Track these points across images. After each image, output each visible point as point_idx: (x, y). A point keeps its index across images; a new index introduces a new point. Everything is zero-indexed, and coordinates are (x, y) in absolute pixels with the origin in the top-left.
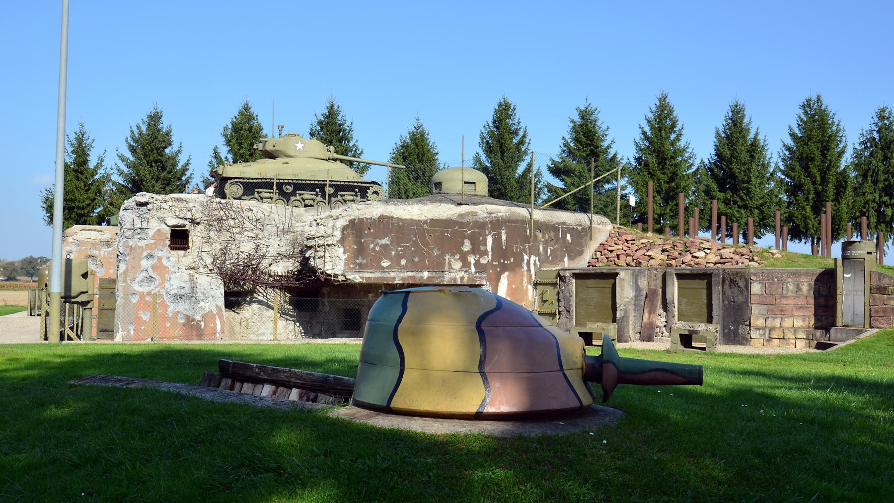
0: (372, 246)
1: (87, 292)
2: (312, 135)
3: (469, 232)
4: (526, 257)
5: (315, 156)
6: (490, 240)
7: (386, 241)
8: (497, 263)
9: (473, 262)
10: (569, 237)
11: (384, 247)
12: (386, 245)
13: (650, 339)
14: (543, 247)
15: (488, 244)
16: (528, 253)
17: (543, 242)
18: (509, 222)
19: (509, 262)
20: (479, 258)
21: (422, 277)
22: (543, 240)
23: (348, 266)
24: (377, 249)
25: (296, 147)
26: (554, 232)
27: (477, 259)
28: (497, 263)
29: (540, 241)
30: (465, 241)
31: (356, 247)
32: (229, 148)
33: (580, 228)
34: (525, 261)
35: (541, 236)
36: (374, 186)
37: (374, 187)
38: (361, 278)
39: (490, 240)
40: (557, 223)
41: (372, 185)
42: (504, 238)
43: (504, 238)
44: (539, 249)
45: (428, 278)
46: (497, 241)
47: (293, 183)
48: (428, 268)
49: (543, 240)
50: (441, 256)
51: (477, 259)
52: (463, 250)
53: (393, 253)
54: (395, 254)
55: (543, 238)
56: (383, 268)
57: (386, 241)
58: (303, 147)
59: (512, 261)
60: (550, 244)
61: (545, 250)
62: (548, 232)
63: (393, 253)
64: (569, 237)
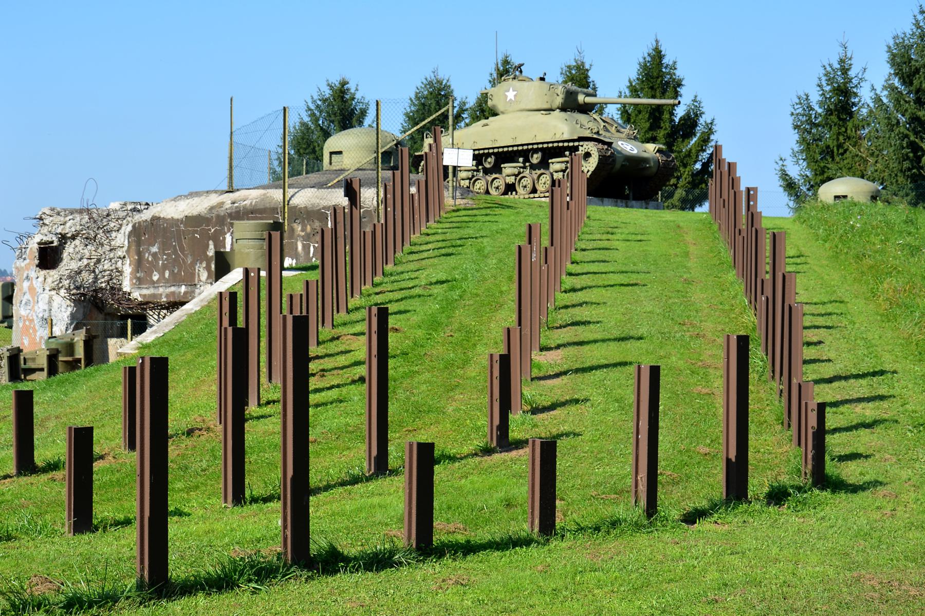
0: (147, 255)
1: (728, 336)
5: (535, 107)
11: (155, 255)
13: (365, 379)
14: (303, 244)
15: (226, 246)
17: (303, 237)
18: (252, 213)
21: (180, 293)
22: (303, 234)
26: (320, 221)
29: (299, 236)
35: (300, 229)
36: (585, 143)
37: (585, 146)
40: (324, 208)
41: (581, 143)
44: (297, 248)
45: (185, 293)
47: (493, 153)
48: (184, 281)
49: (303, 234)
50: (193, 264)
52: (208, 256)
53: (161, 262)
55: (302, 231)
58: (511, 99)
60: (313, 240)
61: (306, 248)
62: (311, 222)
63: (161, 262)
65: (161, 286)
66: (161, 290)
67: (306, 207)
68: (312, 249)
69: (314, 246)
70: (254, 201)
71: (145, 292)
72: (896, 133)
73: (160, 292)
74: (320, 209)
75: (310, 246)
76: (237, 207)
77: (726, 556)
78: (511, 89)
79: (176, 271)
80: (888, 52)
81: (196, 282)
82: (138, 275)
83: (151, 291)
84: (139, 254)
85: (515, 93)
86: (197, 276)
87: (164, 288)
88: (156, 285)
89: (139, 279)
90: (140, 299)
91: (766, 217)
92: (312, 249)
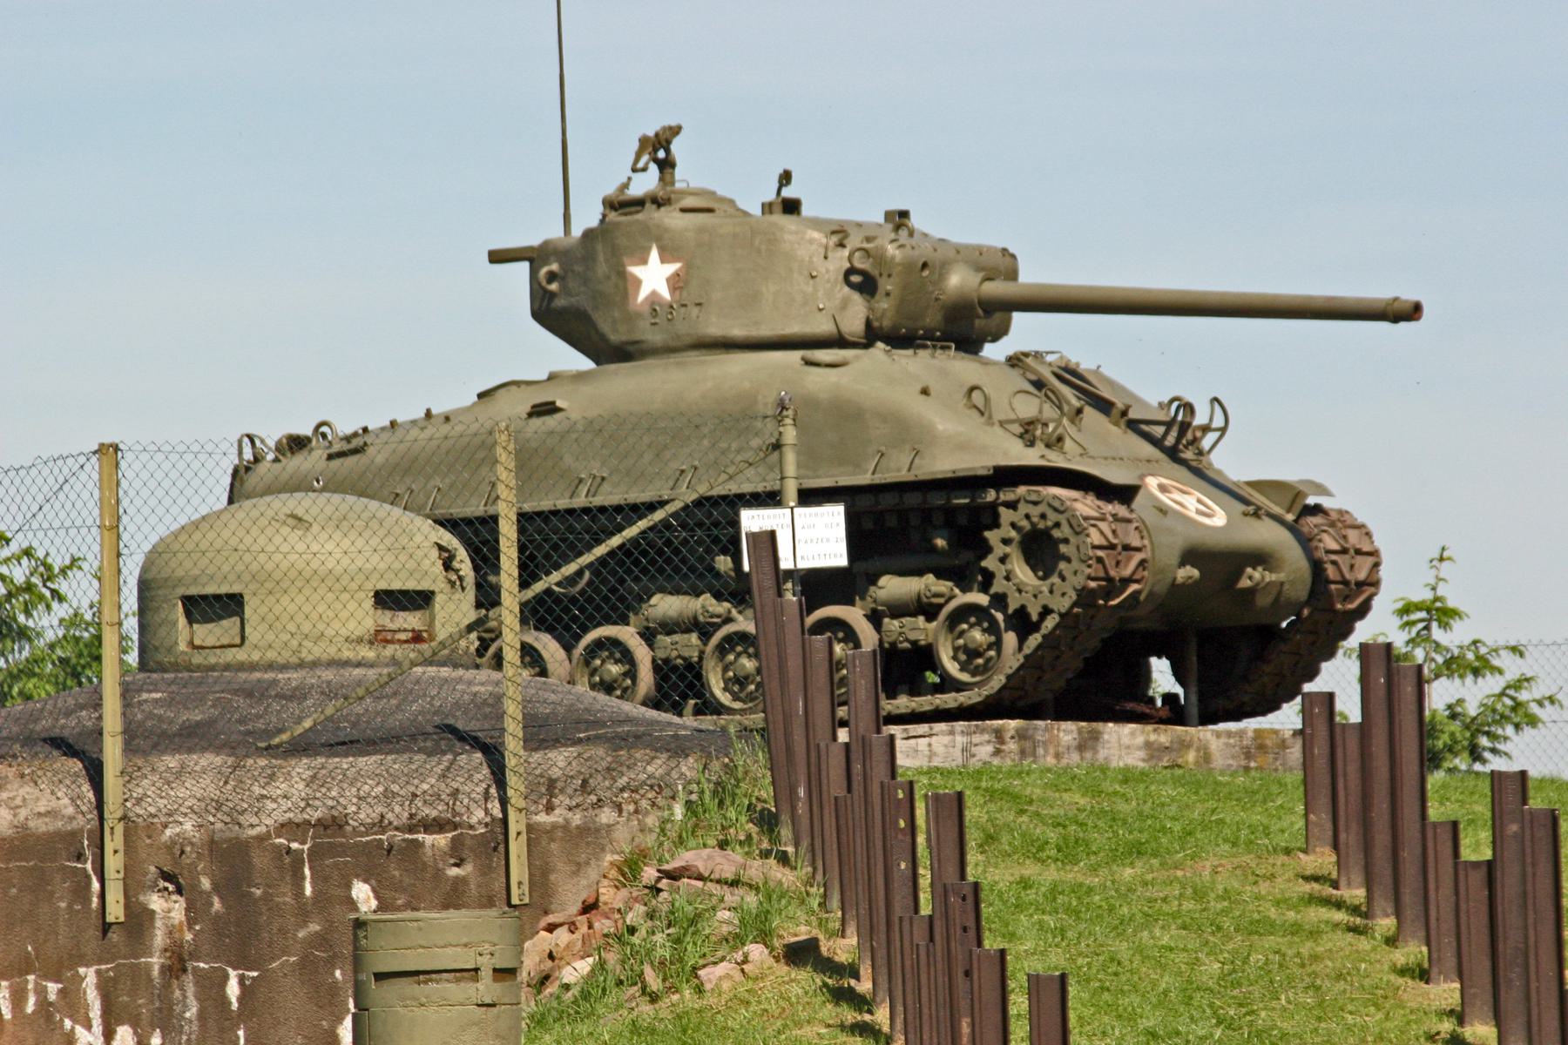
25: (675, 282)
69: (241, 979)
85: (673, 268)
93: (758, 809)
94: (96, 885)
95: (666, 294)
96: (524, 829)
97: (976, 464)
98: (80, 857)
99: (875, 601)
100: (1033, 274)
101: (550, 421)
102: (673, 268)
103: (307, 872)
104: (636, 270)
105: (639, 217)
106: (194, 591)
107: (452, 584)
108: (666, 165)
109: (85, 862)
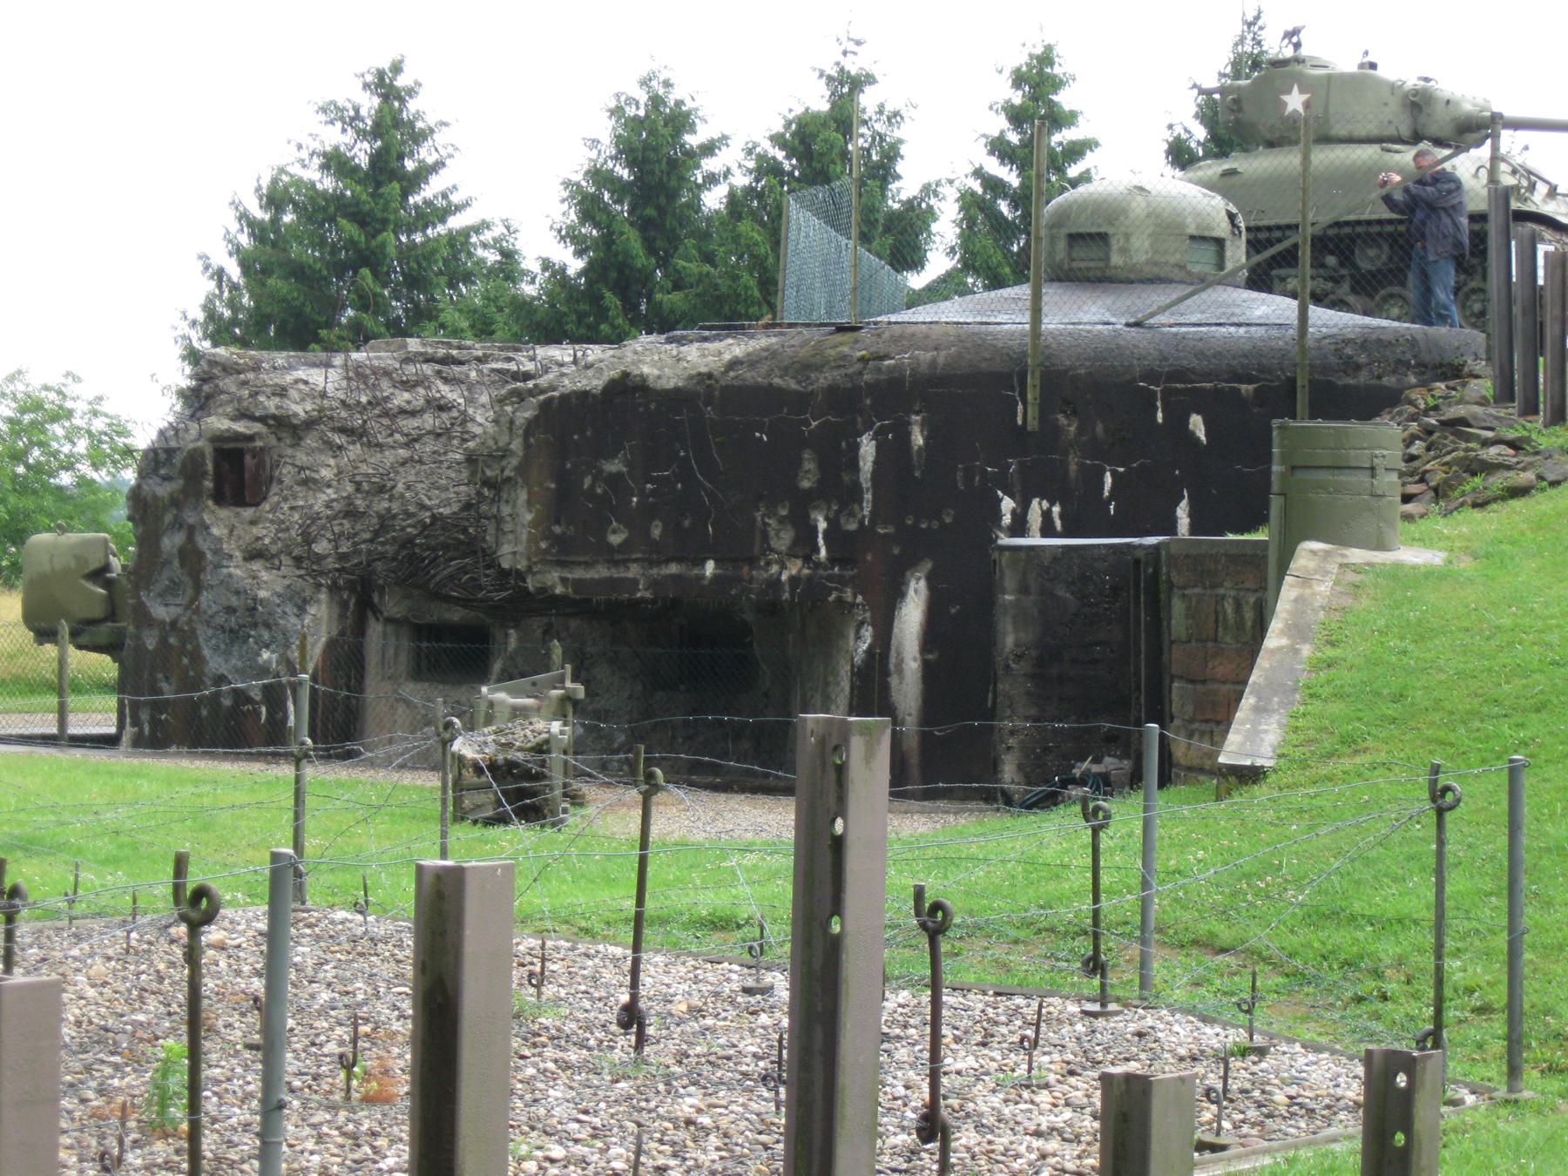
0: (587, 482)
2: (617, 112)
3: (814, 424)
4: (1007, 504)
6: (868, 449)
7: (614, 466)
8: (890, 530)
9: (822, 525)
10: (1197, 424)
11: (615, 480)
12: (619, 476)
16: (1017, 488)
19: (936, 525)
20: (838, 513)
21: (1004, 592)
23: (537, 543)
24: (599, 491)
25: (1307, 105)
27: (831, 516)
28: (890, 530)
30: (807, 455)
31: (553, 486)
32: (1017, 98)
33: (1246, 389)
34: (1007, 520)
38: (564, 581)
39: (868, 449)
42: (918, 439)
43: (918, 439)
46: (893, 451)
51: (831, 516)
54: (637, 503)
56: (610, 546)
57: (614, 466)
59: (948, 520)
64: (1197, 424)
65: (636, 561)
66: (634, 571)
67: (1090, 374)
68: (1108, 479)
69: (1114, 474)
70: (943, 353)
71: (579, 573)
72: (203, 632)
73: (630, 575)
74: (1134, 380)
75: (1104, 471)
76: (891, 369)
77: (1527, 1094)
78: (1296, 88)
79: (687, 523)
80: (1019, 80)
81: (756, 550)
82: (557, 530)
83: (601, 572)
84: (561, 477)
85: (1305, 97)
86: (758, 535)
87: (646, 564)
88: (617, 557)
89: (558, 541)
90: (559, 590)
91: (426, 819)
92: (1108, 479)
93: (256, 695)
94: (1020, 407)
95: (1301, 110)
96: (1306, 383)
97: (185, 763)
98: (1012, 388)
99: (1404, 299)
100: (1510, 112)
101: (1235, 179)
102: (1305, 97)
103: (1159, 404)
104: (1285, 98)
105: (1286, 69)
106: (1074, 230)
107: (1234, 234)
108: (1297, 46)
109: (1014, 391)
